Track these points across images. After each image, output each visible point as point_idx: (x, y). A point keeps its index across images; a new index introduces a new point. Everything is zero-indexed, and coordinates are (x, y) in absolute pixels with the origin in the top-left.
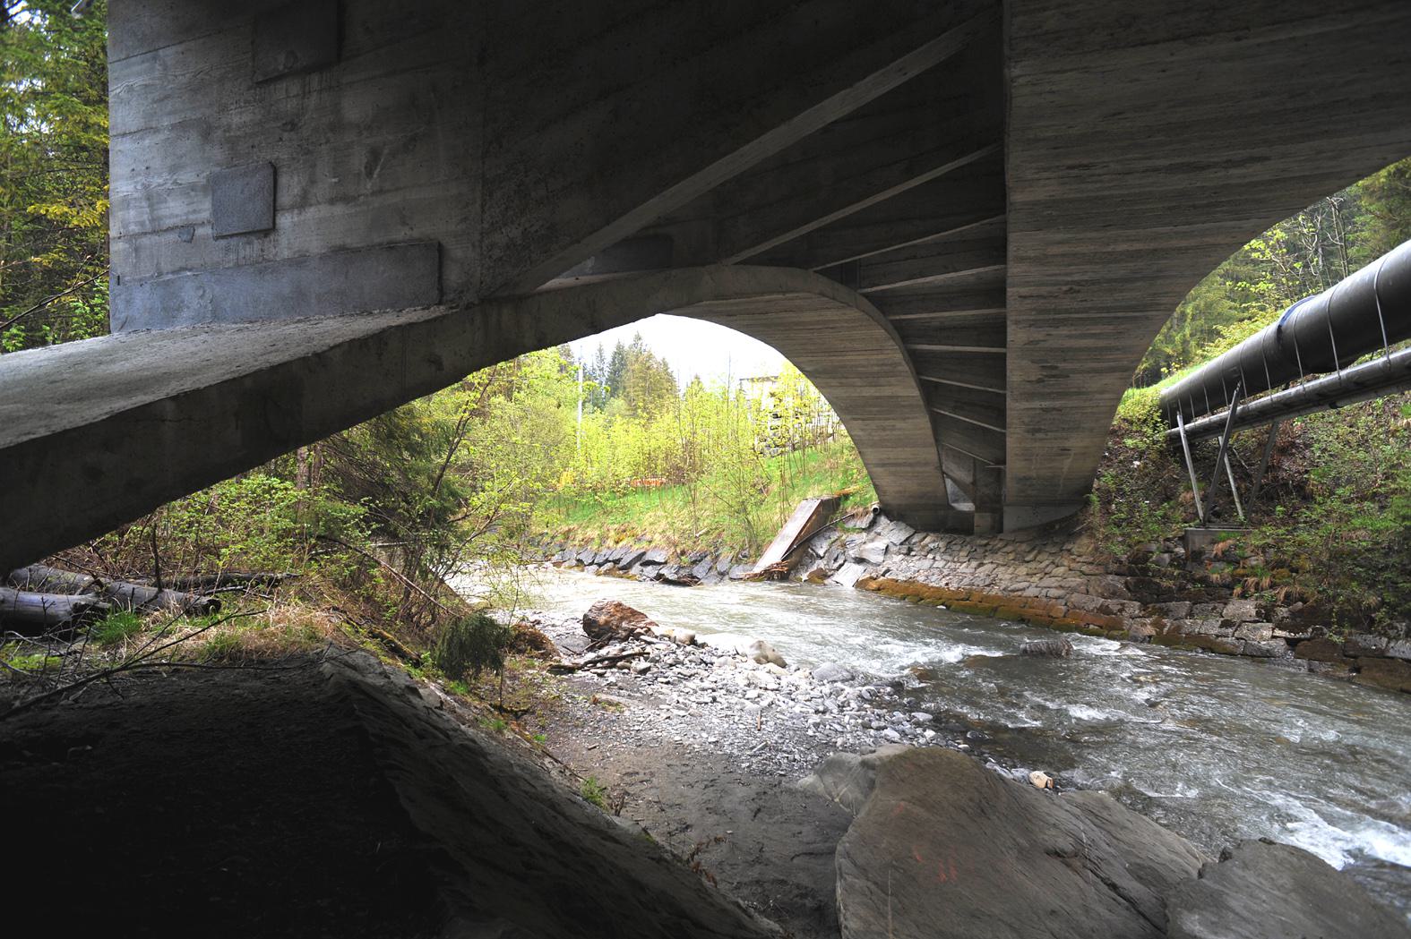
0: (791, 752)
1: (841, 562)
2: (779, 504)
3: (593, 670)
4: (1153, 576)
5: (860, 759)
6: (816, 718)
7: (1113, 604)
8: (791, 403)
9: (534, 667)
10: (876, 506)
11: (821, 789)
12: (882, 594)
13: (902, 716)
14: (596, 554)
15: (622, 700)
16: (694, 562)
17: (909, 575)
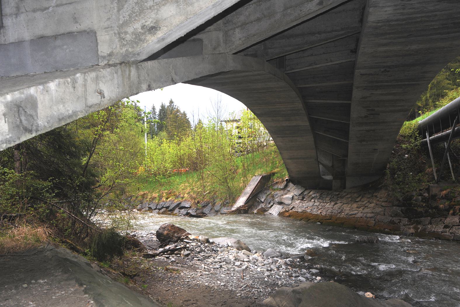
0: (259, 288)
1: (272, 204)
2: (242, 178)
3: (164, 256)
4: (414, 207)
5: (292, 289)
6: (267, 273)
7: (396, 220)
8: (245, 131)
9: (136, 256)
11: (274, 303)
12: (291, 218)
13: (305, 271)
14: (157, 205)
15: (179, 268)
16: (204, 207)
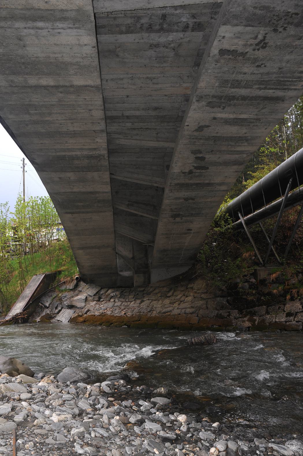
1: (59, 308)
2: (19, 282)
10: (77, 276)
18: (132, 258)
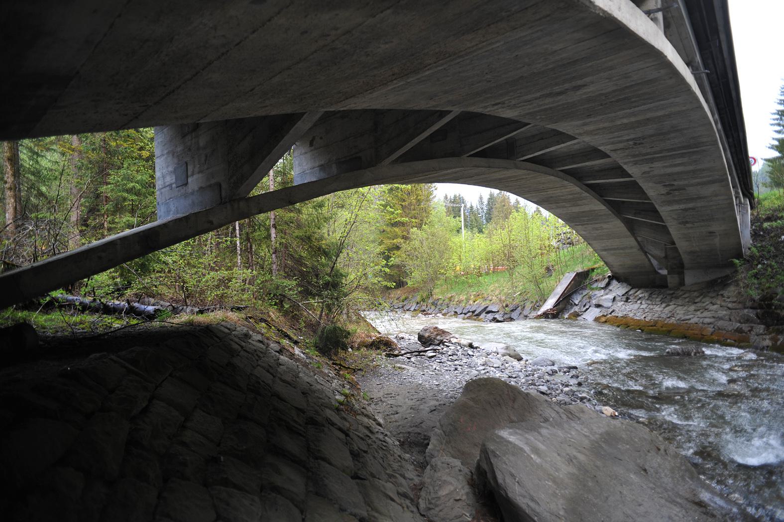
1: (587, 307)
7: (746, 327)
16: (512, 311)
17: (625, 313)
18: (664, 257)
